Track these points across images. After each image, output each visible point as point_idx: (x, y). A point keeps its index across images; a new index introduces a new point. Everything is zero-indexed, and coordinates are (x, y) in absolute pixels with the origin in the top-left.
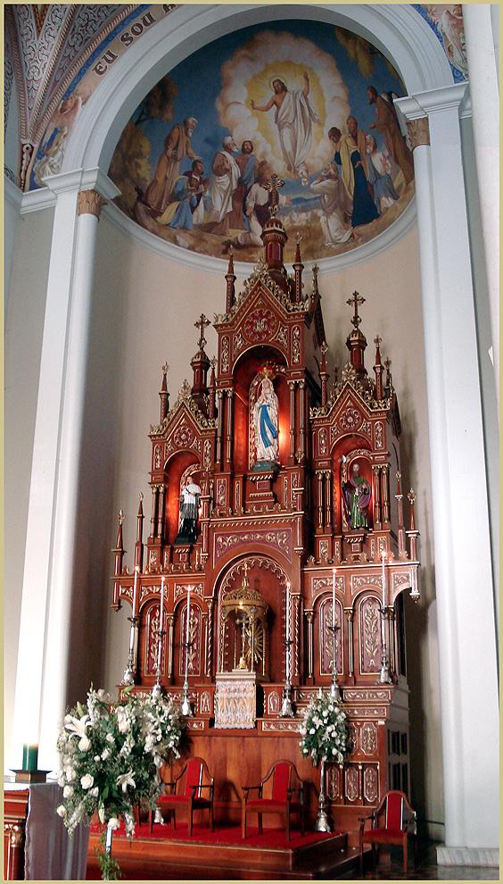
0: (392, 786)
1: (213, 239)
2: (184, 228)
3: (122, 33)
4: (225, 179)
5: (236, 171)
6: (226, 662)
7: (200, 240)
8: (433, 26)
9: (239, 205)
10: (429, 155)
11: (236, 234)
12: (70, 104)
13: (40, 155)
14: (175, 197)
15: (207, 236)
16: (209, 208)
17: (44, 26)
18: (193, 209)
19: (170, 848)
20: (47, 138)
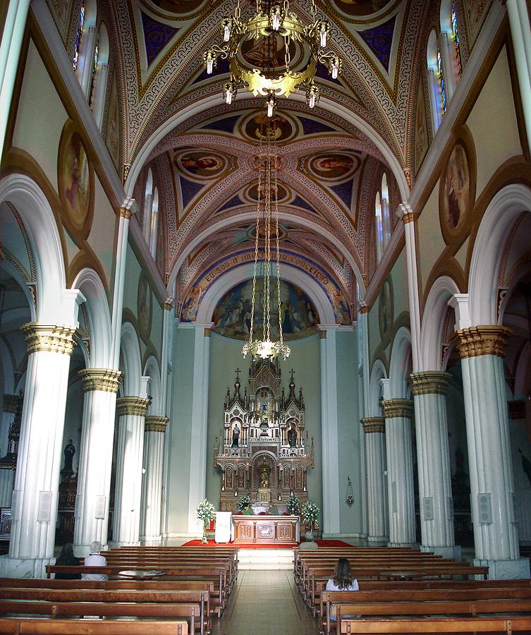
0: (226, 133)
1: (231, 331)
2: (223, 327)
3: (217, 266)
4: (238, 310)
5: (242, 308)
6: (206, 623)
7: (227, 331)
8: (329, 297)
9: (241, 318)
10: (326, 341)
11: (238, 328)
12: (196, 290)
13: (184, 307)
14: (221, 317)
15: (229, 329)
16: (231, 319)
17: (172, 57)
18: (226, 320)
19: (400, 492)
20: (187, 301)
